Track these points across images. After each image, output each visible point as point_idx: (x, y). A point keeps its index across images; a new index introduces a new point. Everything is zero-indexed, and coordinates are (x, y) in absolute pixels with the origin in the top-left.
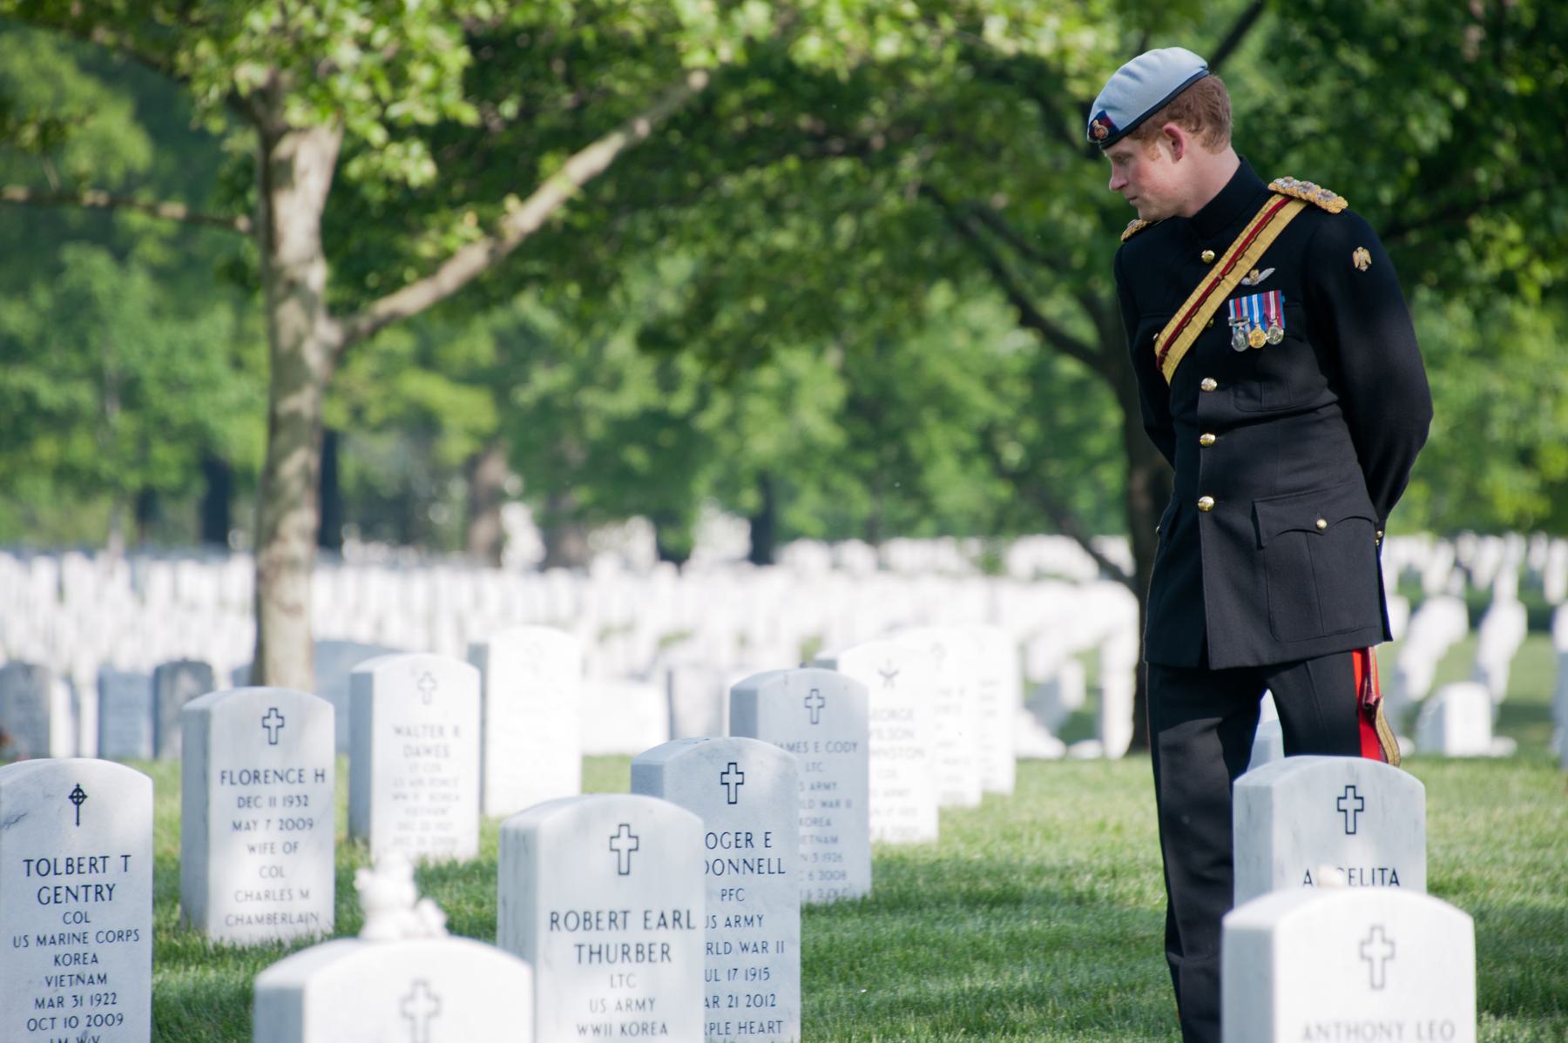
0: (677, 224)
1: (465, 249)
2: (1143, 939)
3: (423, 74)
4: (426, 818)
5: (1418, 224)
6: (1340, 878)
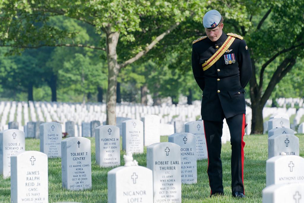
0: (175, 48)
1: (140, 53)
2: (253, 165)
3: (133, 23)
4: (135, 146)
5: (297, 46)
6: (285, 154)
